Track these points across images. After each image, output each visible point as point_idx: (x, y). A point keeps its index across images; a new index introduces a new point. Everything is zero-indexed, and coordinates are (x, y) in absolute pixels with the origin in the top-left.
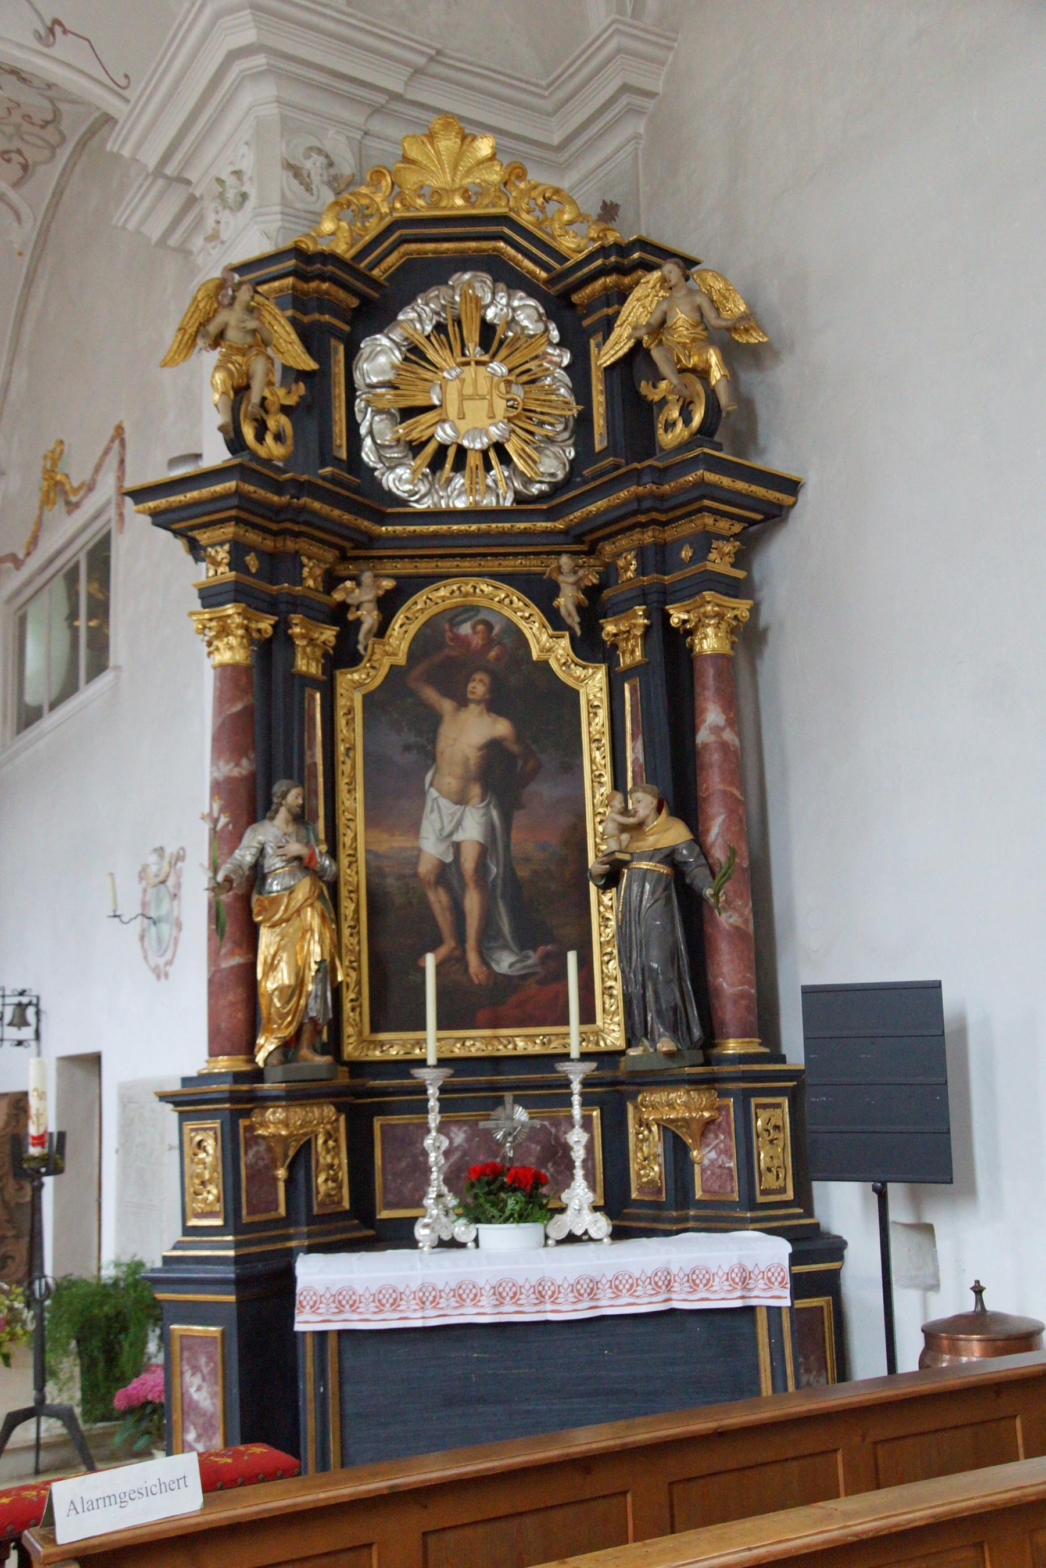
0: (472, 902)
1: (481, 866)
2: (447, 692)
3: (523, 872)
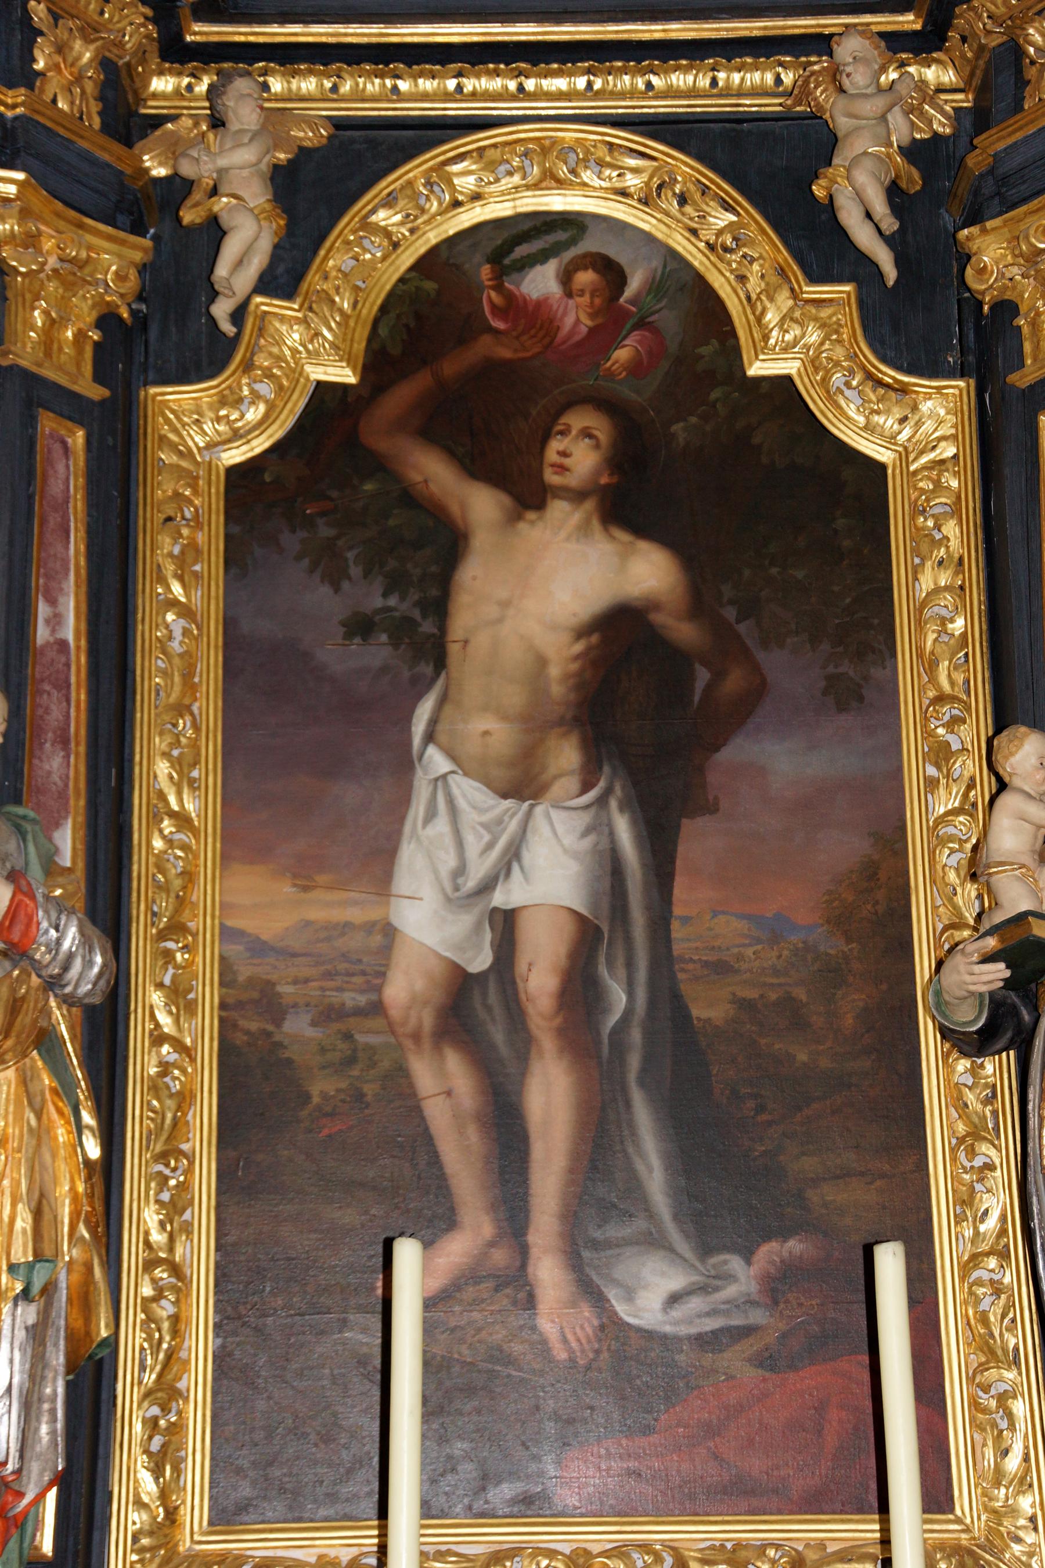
0: (550, 1096)
1: (580, 989)
2: (478, 466)
3: (708, 1008)
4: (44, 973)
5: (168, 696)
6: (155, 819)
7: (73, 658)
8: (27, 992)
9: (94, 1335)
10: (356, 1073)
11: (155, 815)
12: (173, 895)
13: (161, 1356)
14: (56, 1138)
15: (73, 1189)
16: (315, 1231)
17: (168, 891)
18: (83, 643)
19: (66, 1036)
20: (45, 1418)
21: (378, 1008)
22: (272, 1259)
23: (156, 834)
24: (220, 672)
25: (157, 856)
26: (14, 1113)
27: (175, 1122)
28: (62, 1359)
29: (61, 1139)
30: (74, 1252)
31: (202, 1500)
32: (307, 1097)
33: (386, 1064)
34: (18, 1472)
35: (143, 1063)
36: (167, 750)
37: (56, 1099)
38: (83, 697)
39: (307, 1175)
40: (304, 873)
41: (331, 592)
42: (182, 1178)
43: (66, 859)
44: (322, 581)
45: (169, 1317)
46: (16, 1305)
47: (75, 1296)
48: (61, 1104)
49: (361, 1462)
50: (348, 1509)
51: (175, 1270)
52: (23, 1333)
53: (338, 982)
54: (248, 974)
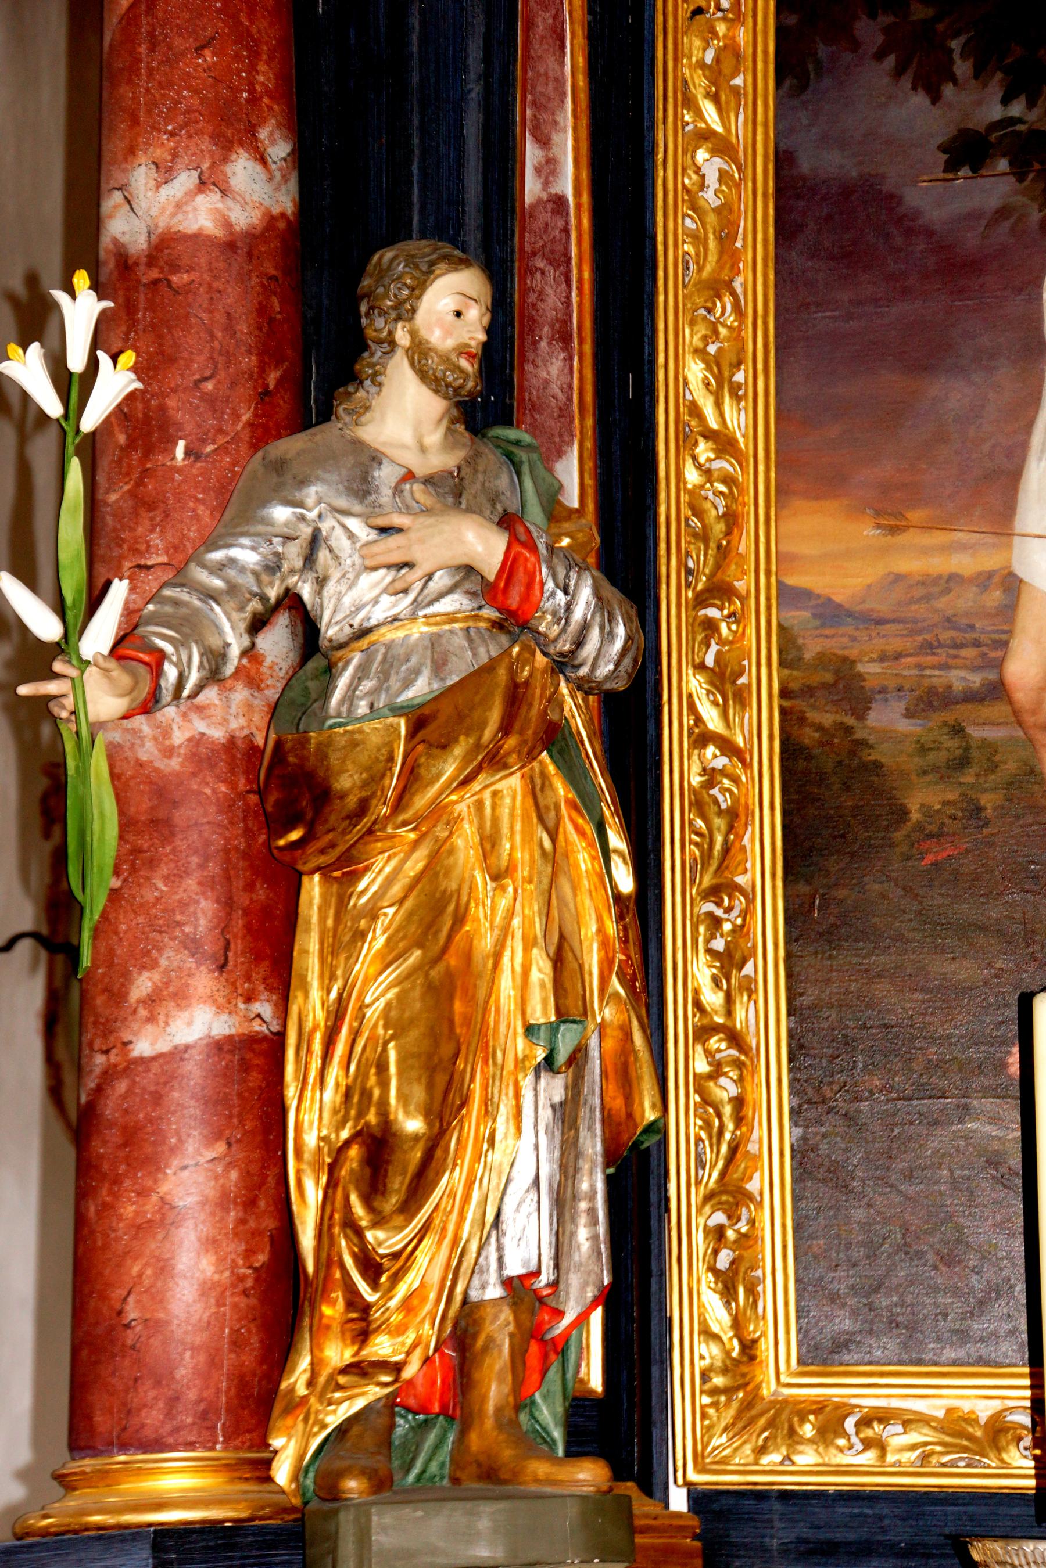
4: (551, 650)
5: (700, 270)
6: (685, 442)
7: (573, 221)
8: (531, 675)
9: (638, 1120)
10: (970, 779)
11: (686, 437)
12: (713, 545)
13: (724, 1149)
14: (577, 865)
15: (601, 930)
16: (922, 990)
17: (706, 539)
18: (585, 198)
19: (584, 734)
20: (583, 1220)
21: (998, 690)
22: (864, 1027)
23: (689, 462)
24: (771, 231)
25: (691, 493)
26: (523, 832)
27: (726, 850)
28: (599, 1147)
29: (583, 867)
30: (607, 1012)
31: (788, 1332)
32: (902, 814)
33: (1011, 766)
34: (555, 1284)
35: (682, 769)
36: (701, 345)
37: (574, 814)
38: (586, 275)
39: (907, 917)
40: (891, 511)
41: (928, 102)
42: (739, 921)
43: (572, 499)
44: (914, 88)
45: (730, 1100)
46: (537, 1077)
47: (610, 1069)
48: (580, 821)
49: (997, 1291)
50: (984, 1350)
51: (735, 1039)
52: (549, 1112)
53: (942, 656)
54: (819, 649)
